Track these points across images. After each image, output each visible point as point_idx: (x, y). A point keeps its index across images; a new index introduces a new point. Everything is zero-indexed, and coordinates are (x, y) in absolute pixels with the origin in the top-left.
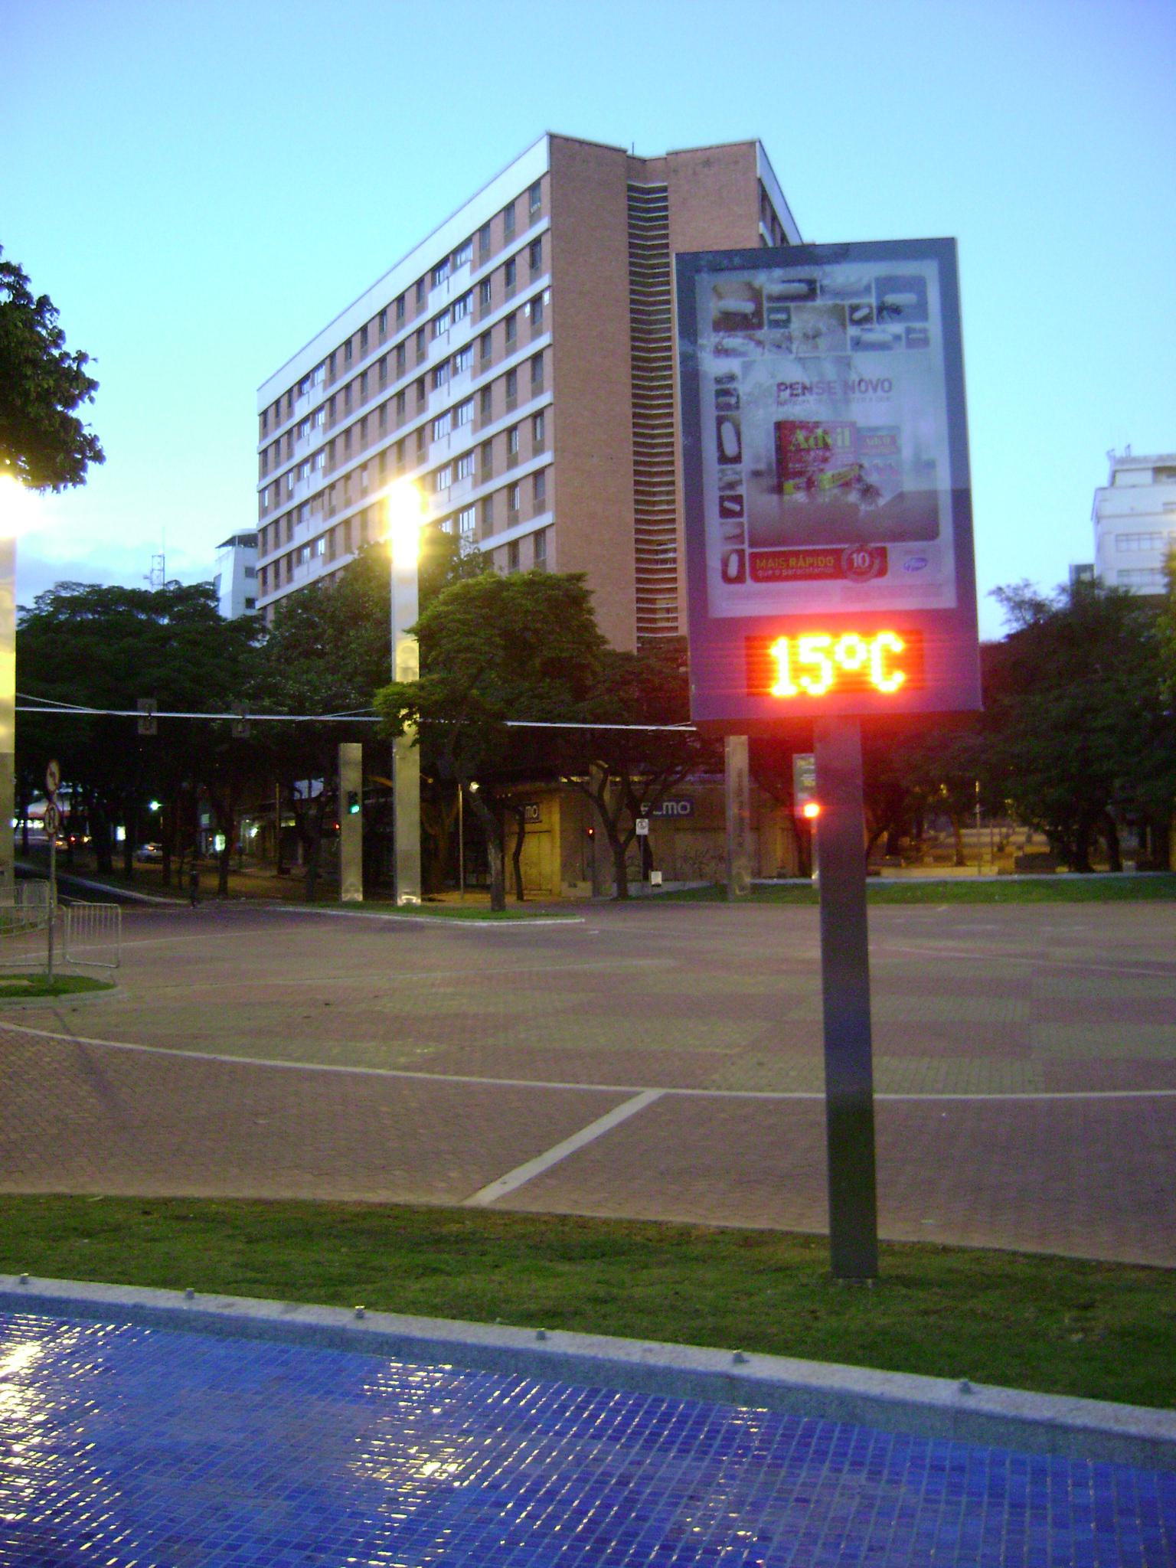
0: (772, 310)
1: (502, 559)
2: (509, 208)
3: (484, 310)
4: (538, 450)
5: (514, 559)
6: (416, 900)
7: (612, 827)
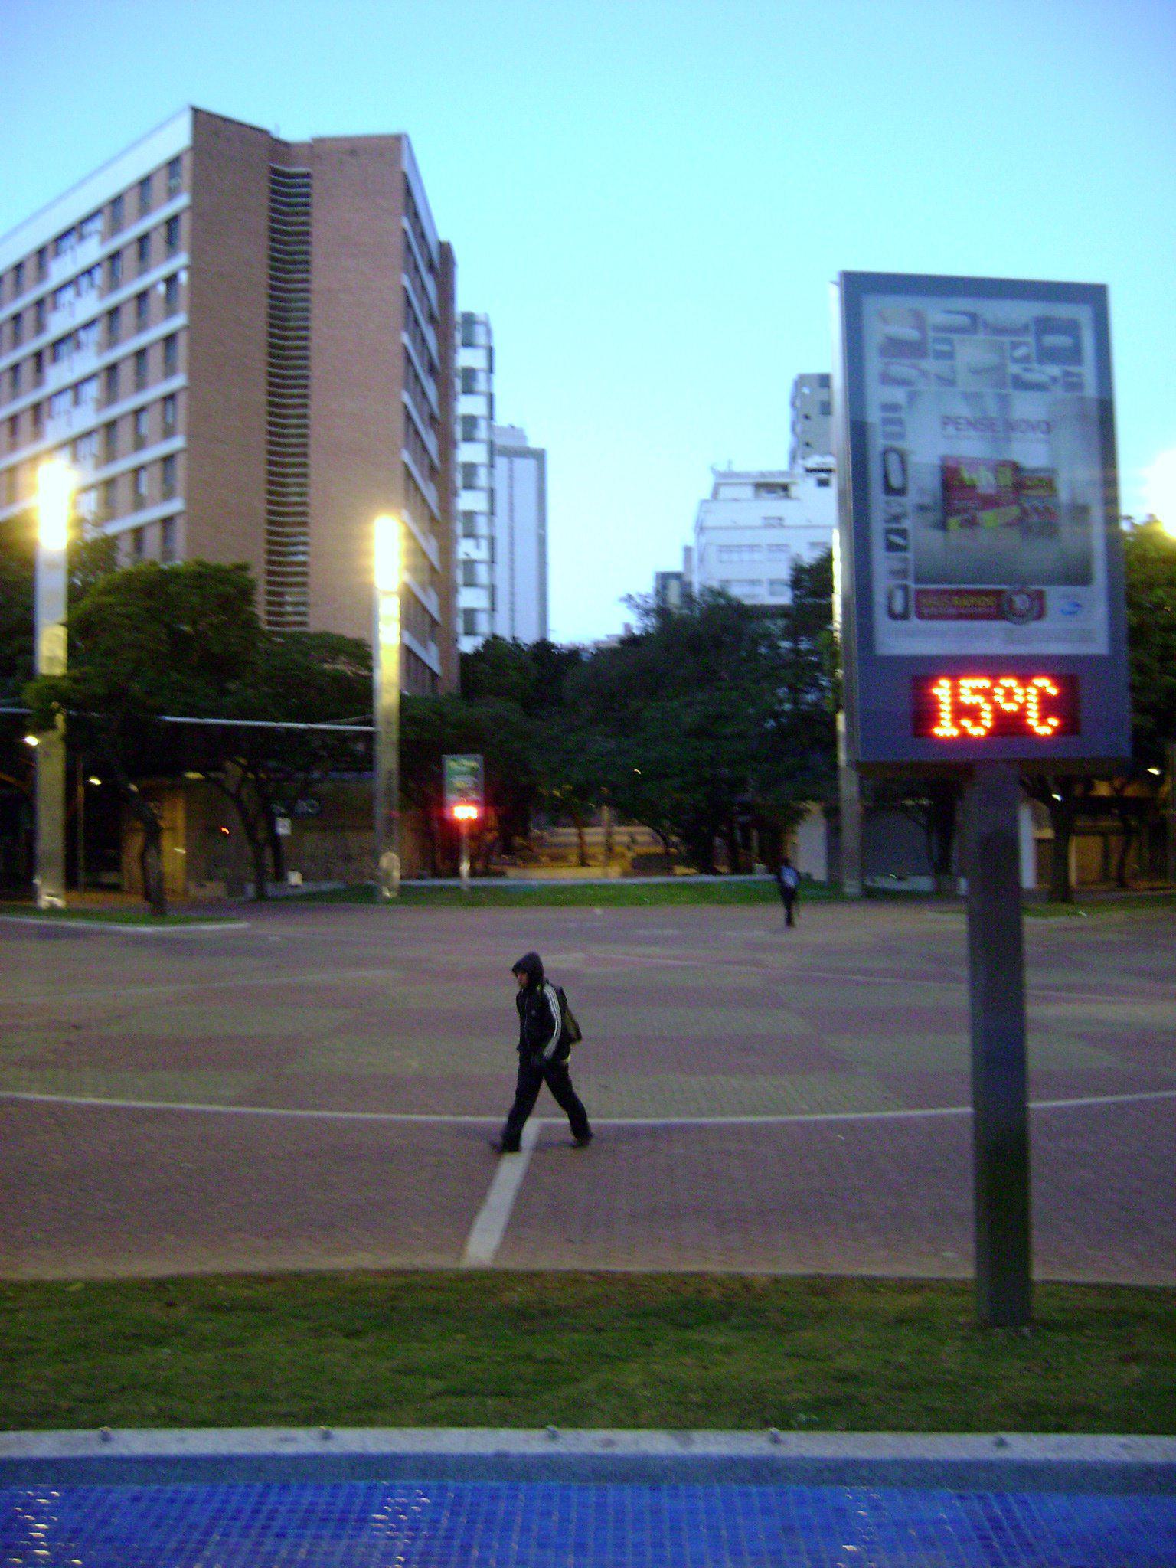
0: (937, 340)
1: (126, 545)
2: (145, 183)
3: (114, 282)
4: (168, 433)
5: (166, 538)
6: (59, 902)
7: (251, 829)
